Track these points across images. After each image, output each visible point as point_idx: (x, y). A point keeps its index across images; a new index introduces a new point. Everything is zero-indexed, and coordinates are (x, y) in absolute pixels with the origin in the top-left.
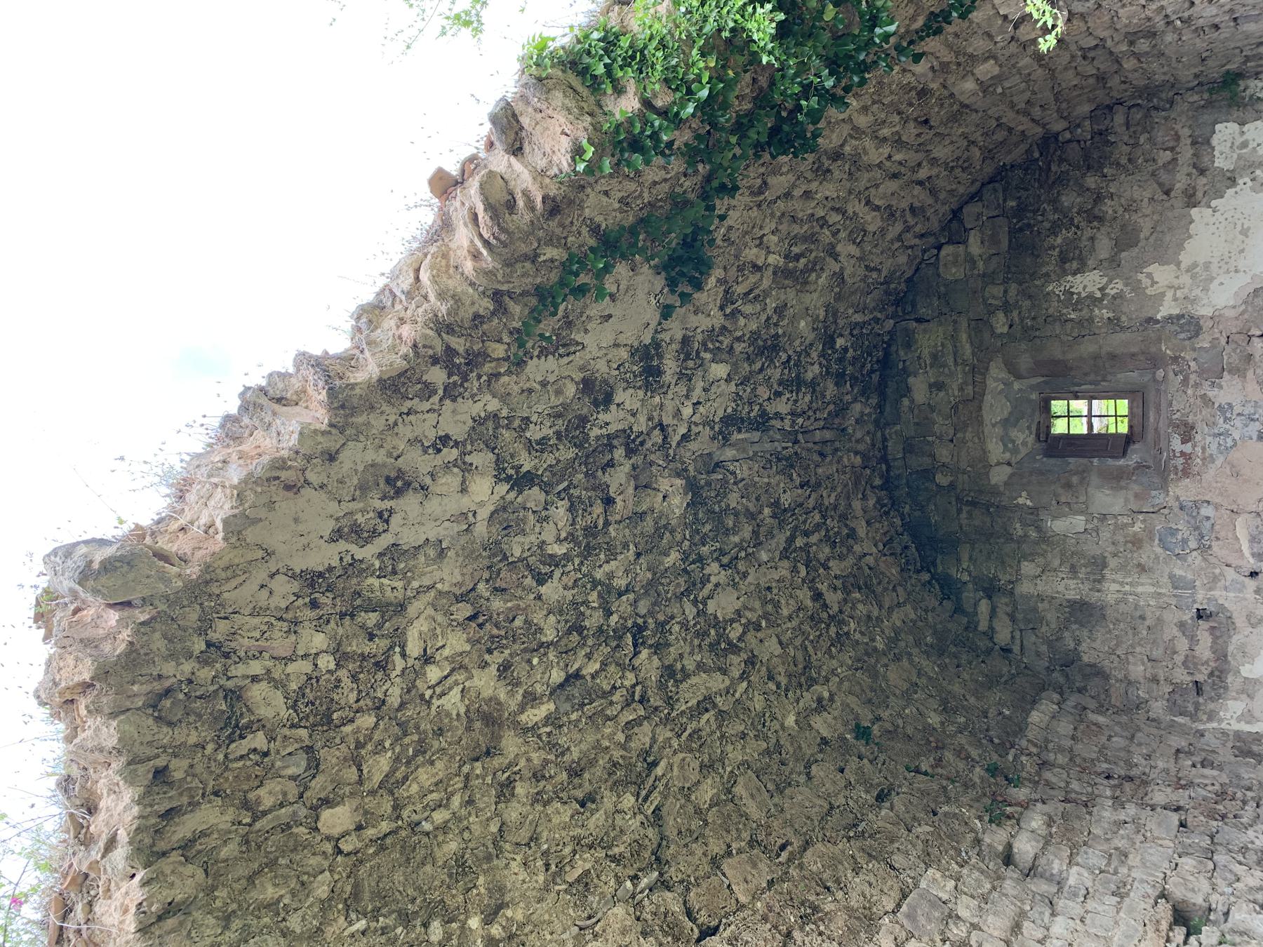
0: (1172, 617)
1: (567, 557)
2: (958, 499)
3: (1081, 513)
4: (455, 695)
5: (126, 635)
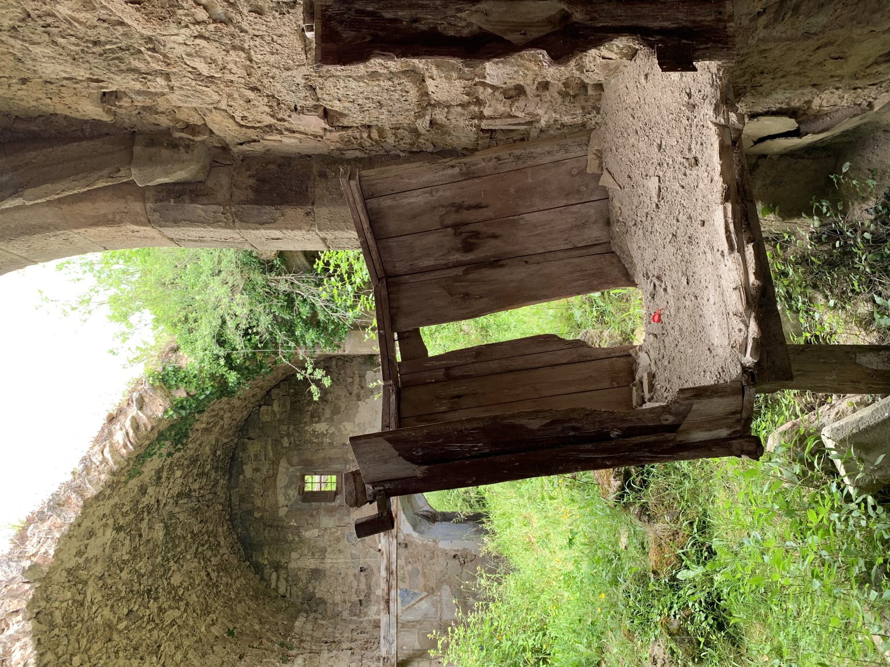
0: (351, 572)
1: (128, 560)
2: (264, 524)
3: (317, 528)
4: (99, 618)
5: (31, 592)
